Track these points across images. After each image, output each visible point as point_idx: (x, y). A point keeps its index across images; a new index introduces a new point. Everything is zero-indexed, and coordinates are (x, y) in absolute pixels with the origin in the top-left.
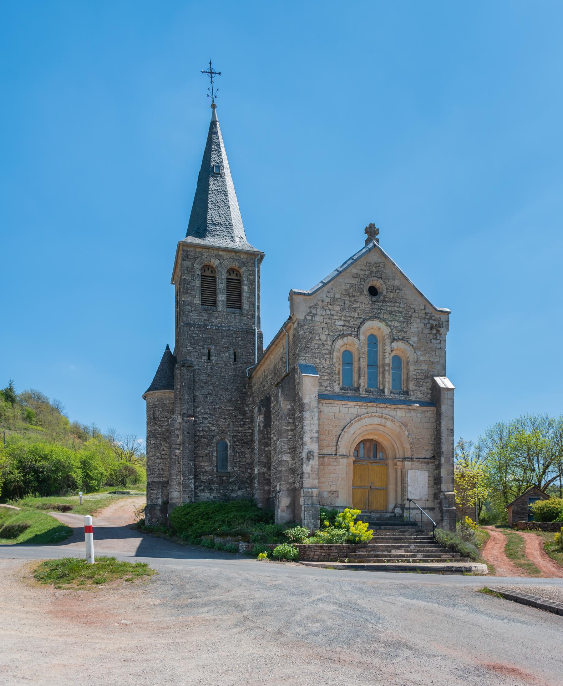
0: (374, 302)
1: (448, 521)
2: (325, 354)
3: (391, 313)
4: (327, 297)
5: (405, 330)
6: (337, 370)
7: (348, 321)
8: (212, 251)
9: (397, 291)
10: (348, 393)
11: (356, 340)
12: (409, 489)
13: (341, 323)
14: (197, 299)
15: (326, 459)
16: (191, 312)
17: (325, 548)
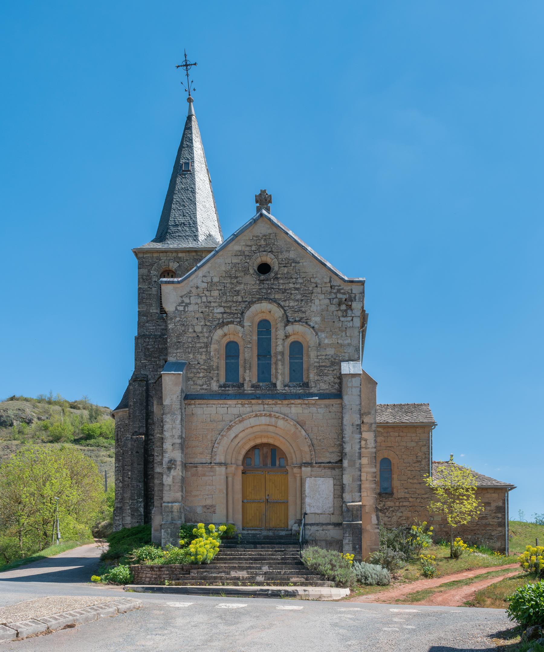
0: (262, 281)
1: (351, 538)
2: (201, 347)
3: (284, 291)
4: (203, 282)
5: (303, 309)
6: (215, 364)
7: (230, 307)
8: (170, 254)
9: (293, 265)
10: (228, 390)
11: (239, 328)
12: (307, 500)
13: (221, 310)
14: (153, 308)
15: (200, 469)
16: (147, 322)
17: (155, 569)
